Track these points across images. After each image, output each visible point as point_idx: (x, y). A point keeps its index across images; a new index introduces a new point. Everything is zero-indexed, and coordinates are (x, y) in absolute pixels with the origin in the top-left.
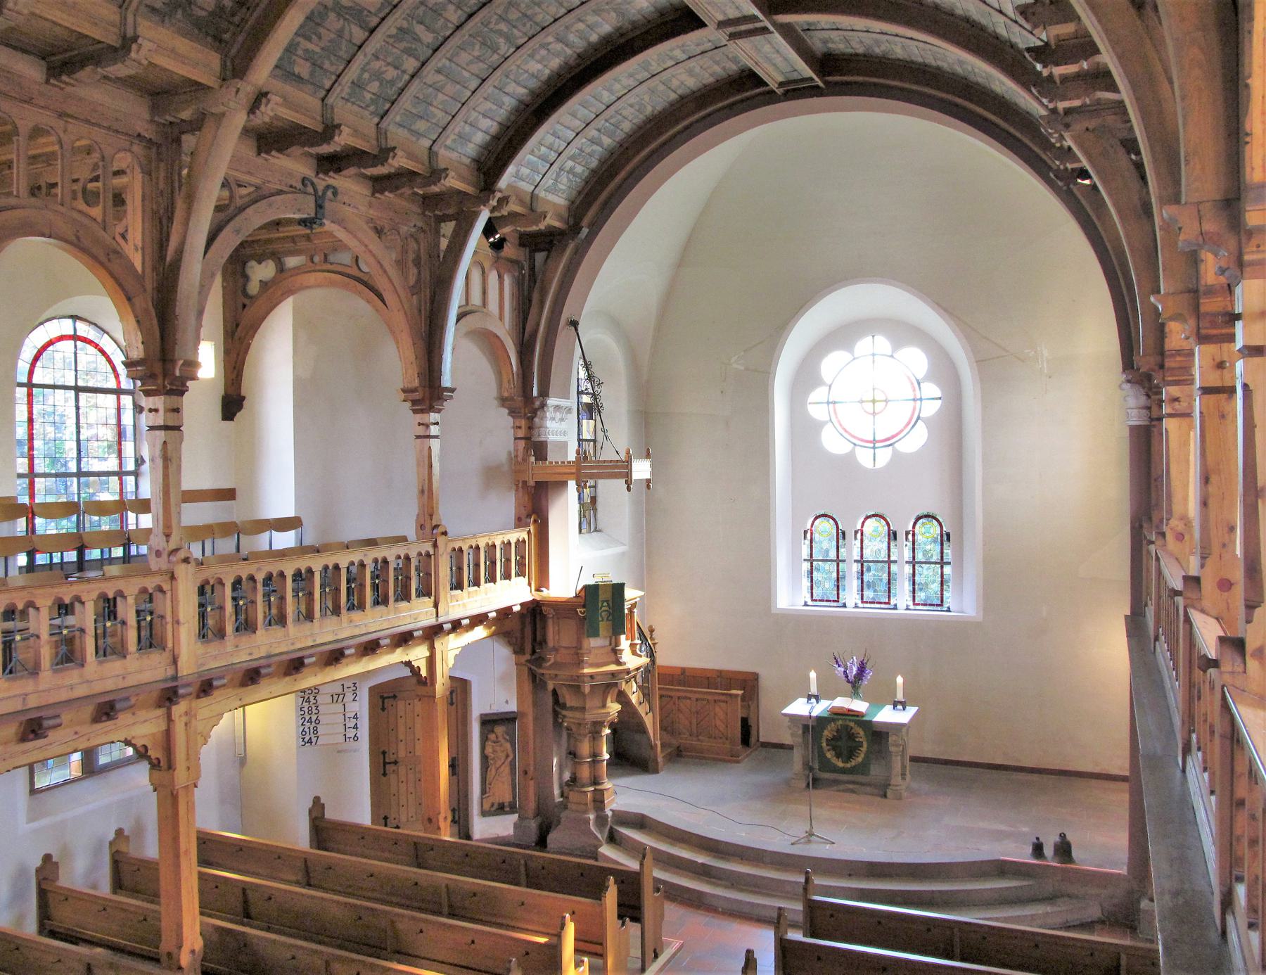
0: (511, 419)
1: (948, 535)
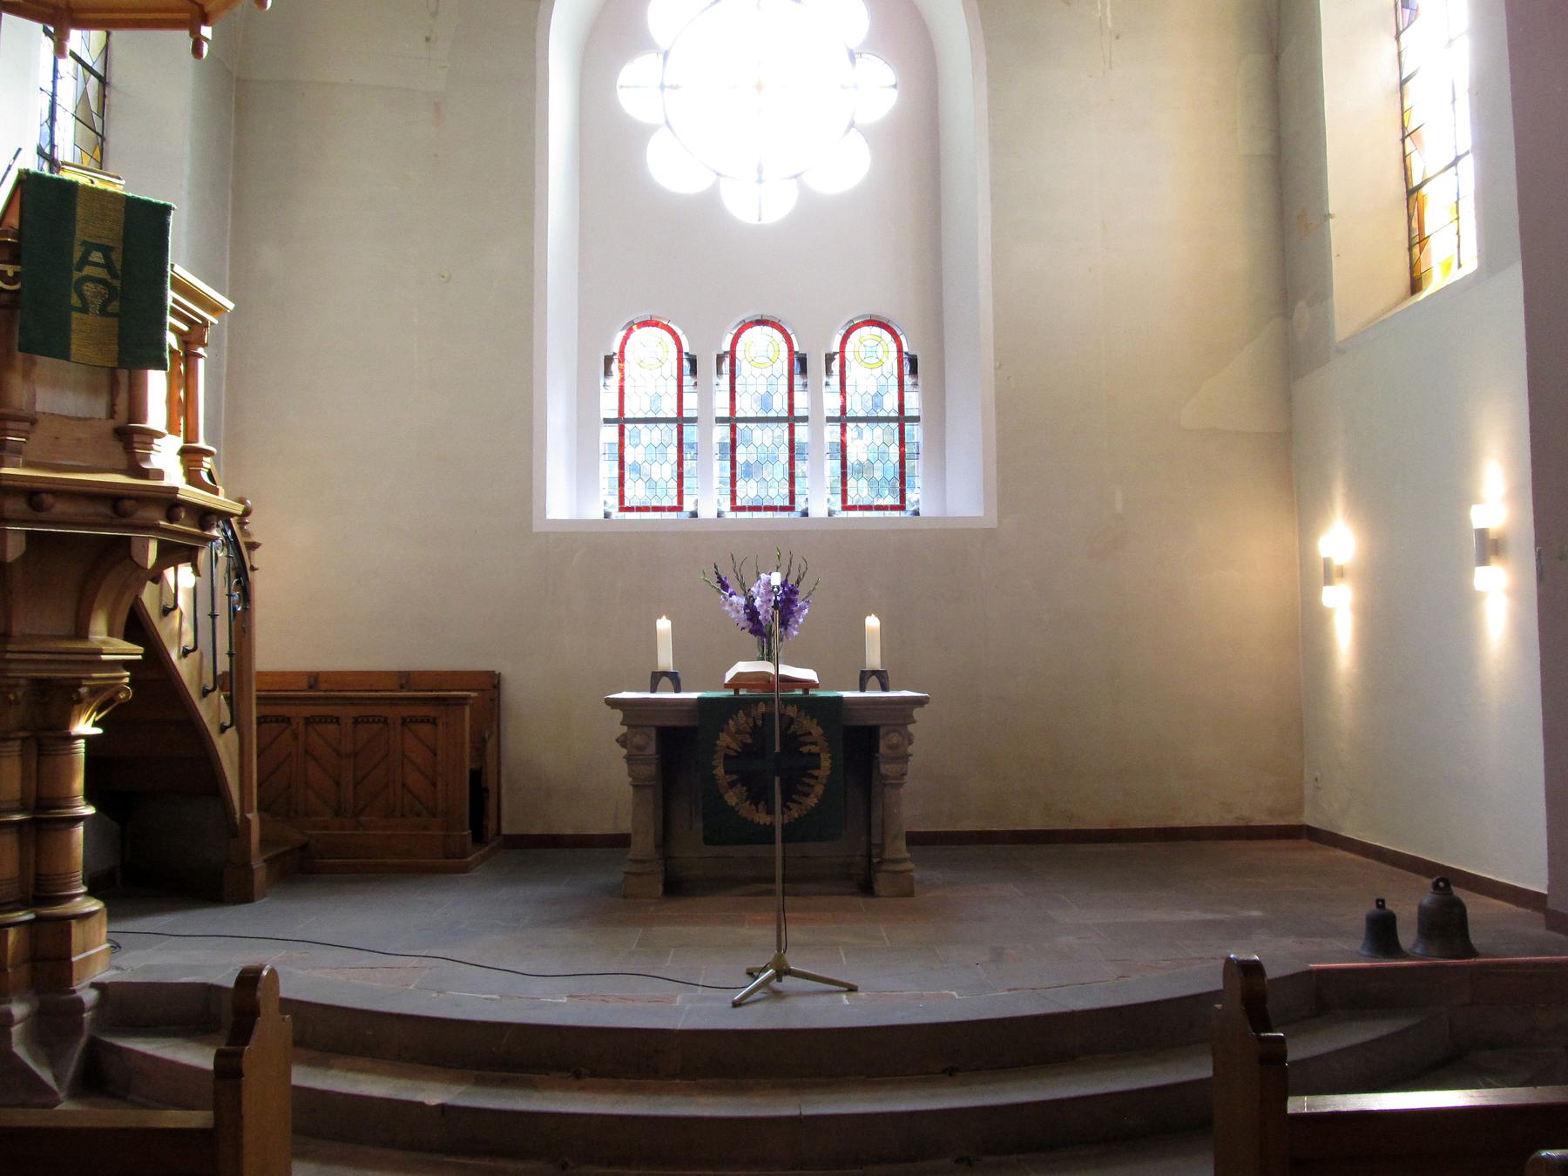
1: (913, 361)
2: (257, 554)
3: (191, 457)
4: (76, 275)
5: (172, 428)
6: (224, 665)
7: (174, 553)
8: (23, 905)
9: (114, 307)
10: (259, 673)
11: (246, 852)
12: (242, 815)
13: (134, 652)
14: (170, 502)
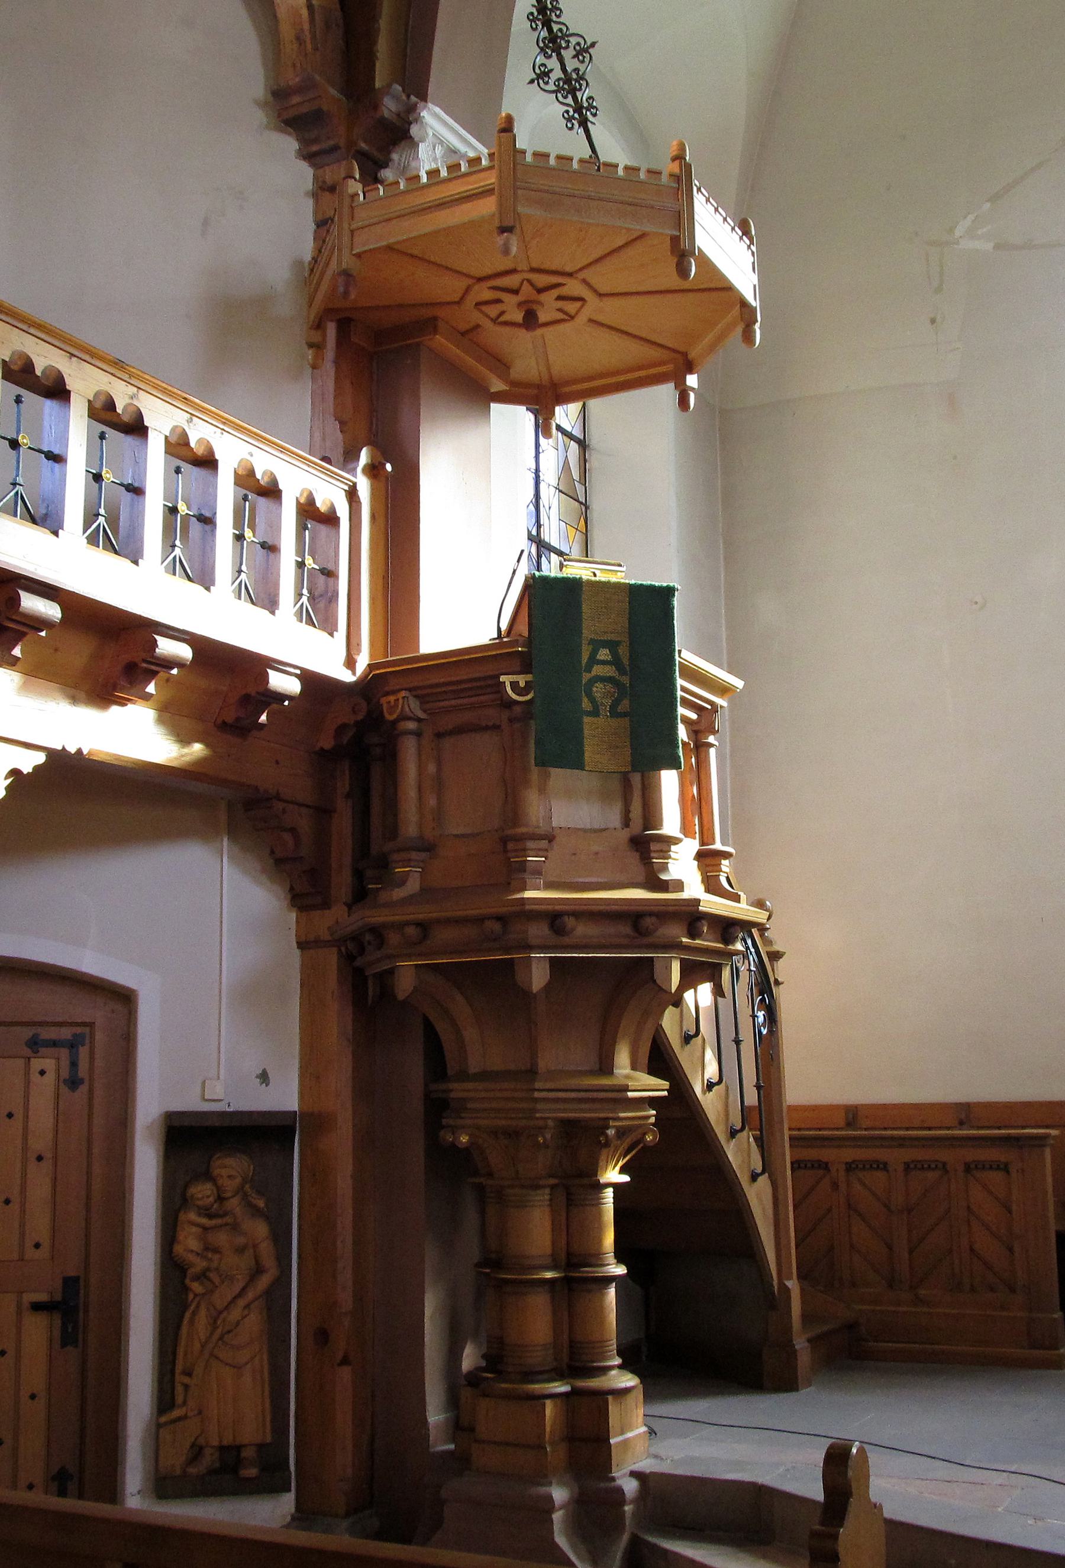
0: (305, 173)
2: (781, 964)
3: (708, 861)
4: (586, 677)
5: (686, 830)
6: (752, 1098)
7: (692, 974)
8: (559, 1375)
9: (625, 705)
10: (792, 1109)
11: (788, 1329)
12: (781, 1284)
13: (657, 1087)
14: (691, 916)
